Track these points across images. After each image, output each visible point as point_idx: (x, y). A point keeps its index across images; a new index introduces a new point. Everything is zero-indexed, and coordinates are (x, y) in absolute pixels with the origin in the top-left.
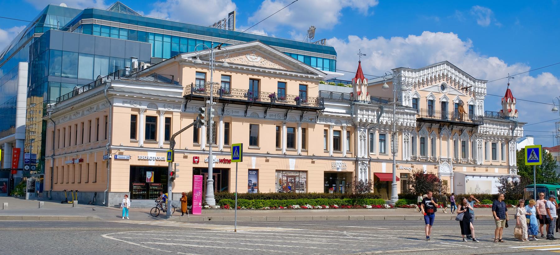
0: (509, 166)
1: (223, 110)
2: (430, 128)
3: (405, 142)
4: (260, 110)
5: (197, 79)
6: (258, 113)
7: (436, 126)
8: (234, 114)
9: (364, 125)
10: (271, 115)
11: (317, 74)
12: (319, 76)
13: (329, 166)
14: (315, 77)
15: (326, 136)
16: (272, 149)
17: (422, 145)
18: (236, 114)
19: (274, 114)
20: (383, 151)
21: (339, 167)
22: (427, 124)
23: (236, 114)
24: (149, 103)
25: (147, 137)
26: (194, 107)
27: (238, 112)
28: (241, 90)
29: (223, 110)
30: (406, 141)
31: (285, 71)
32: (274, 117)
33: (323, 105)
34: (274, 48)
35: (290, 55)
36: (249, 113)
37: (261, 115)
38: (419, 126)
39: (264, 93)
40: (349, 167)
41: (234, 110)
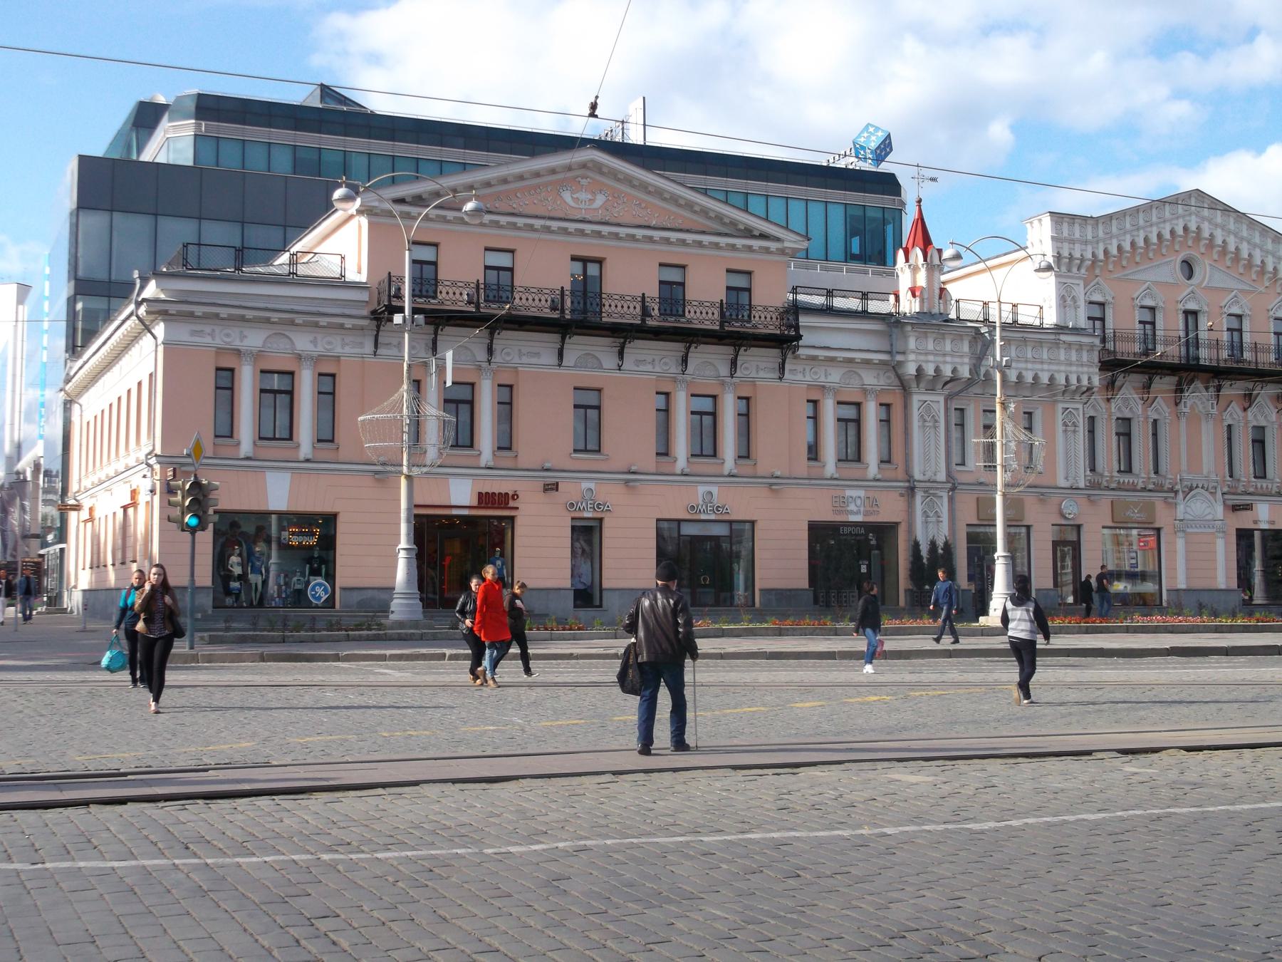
0: (909, 477)
1: (490, 351)
2: (1147, 387)
3: (1065, 431)
4: (602, 349)
5: (728, 288)
6: (597, 354)
7: (1164, 384)
8: (525, 360)
9: (936, 382)
10: (638, 362)
11: (778, 239)
12: (787, 244)
13: (674, 501)
14: (773, 246)
15: (815, 418)
16: (645, 456)
17: (744, 418)
18: (534, 360)
19: (649, 359)
20: (708, 449)
21: (856, 508)
22: (1134, 377)
23: (534, 360)
24: (271, 332)
25: (842, 460)
26: (657, 358)
27: (537, 355)
28: (540, 291)
29: (490, 351)
30: (1070, 427)
31: (726, 235)
32: (649, 368)
33: (797, 328)
34: (667, 178)
35: (705, 192)
36: (569, 358)
37: (609, 360)
38: (1111, 386)
39: (527, 289)
40: (889, 509)
41: (524, 350)
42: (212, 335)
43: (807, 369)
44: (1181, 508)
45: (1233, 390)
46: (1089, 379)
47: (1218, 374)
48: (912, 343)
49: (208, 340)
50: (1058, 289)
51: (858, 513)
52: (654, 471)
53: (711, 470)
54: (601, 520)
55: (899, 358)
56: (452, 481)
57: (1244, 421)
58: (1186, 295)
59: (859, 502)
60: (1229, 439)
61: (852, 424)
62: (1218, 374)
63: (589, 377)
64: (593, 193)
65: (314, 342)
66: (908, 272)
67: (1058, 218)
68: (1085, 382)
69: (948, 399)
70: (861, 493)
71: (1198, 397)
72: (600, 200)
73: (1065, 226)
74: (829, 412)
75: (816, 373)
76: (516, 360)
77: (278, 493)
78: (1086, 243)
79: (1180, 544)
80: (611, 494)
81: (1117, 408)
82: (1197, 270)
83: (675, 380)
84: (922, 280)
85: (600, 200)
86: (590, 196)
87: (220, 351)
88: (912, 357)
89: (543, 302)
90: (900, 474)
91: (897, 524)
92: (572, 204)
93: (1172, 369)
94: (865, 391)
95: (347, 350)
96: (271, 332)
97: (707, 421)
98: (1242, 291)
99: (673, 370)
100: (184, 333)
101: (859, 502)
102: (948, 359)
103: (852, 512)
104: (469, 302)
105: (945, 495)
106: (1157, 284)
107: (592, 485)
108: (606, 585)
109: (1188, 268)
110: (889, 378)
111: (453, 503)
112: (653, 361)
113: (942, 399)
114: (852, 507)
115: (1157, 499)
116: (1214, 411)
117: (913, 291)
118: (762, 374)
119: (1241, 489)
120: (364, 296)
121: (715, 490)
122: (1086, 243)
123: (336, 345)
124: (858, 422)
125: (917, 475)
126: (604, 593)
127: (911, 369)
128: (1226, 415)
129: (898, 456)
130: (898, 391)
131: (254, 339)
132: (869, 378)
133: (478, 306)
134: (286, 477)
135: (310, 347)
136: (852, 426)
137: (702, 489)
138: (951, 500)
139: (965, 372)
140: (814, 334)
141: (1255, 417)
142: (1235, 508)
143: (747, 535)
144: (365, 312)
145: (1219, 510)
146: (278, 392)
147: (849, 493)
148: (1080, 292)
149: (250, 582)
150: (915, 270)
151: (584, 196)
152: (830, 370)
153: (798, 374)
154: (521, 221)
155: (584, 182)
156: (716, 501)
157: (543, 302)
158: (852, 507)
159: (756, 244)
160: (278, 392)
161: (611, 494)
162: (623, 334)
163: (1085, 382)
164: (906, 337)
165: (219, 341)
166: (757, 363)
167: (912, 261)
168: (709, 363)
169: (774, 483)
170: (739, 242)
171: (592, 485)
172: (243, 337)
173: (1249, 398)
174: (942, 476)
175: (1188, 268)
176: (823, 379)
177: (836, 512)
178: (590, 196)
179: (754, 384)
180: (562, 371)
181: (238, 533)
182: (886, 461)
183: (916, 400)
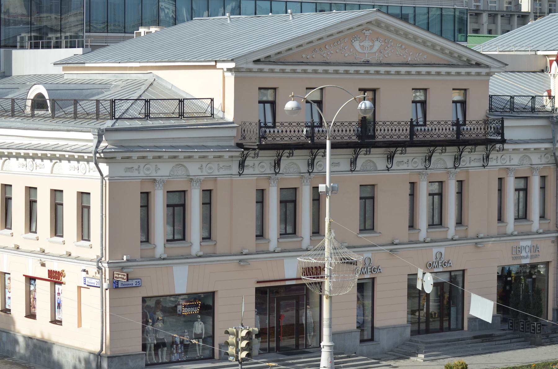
6: (373, 160)
11: (487, 67)
16: (404, 233)
24: (174, 164)
32: (405, 166)
49: (136, 174)
51: (527, 257)
52: (406, 240)
54: (373, 279)
56: (286, 261)
59: (527, 249)
61: (524, 191)
64: (373, 41)
70: (529, 243)
72: (377, 45)
74: (511, 185)
80: (379, 257)
83: (420, 174)
85: (377, 45)
86: (371, 44)
87: (143, 181)
89: (352, 132)
92: (360, 50)
95: (222, 172)
96: (174, 164)
99: (420, 167)
101: (527, 249)
104: (307, 137)
110: (547, 158)
111: (287, 277)
112: (410, 161)
114: (524, 254)
118: (473, 164)
120: (234, 133)
123: (215, 169)
124: (525, 190)
126: (375, 330)
131: (164, 170)
133: (312, 140)
134: (186, 267)
135: (198, 172)
143: (460, 279)
144: (233, 143)
146: (177, 207)
147: (523, 244)
151: (367, 43)
155: (367, 33)
156: (445, 259)
157: (352, 132)
158: (524, 254)
159: (474, 70)
160: (177, 207)
161: (379, 257)
162: (393, 146)
165: (143, 173)
168: (443, 159)
170: (463, 70)
171: (369, 255)
172: (157, 169)
176: (508, 163)
178: (371, 44)
180: (354, 174)
181: (156, 308)
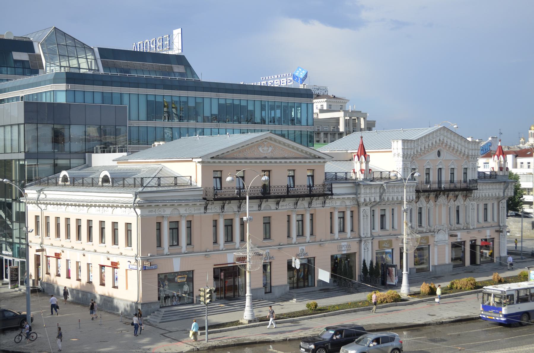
0: (360, 237)
2: (428, 197)
11: (324, 158)
16: (284, 239)
19: (285, 204)
32: (285, 208)
36: (263, 206)
38: (418, 198)
40: (354, 249)
42: (155, 211)
43: (157, 209)
44: (436, 238)
45: (451, 194)
46: (375, 198)
47: (446, 191)
48: (363, 191)
49: (154, 213)
50: (403, 165)
52: (286, 243)
53: (303, 241)
55: (359, 196)
56: (228, 254)
57: (453, 204)
58: (439, 163)
60: (393, 214)
62: (446, 191)
63: (267, 213)
65: (186, 210)
66: (358, 164)
67: (404, 141)
68: (411, 198)
69: (371, 208)
70: (346, 243)
71: (442, 199)
72: (270, 149)
73: (406, 144)
74: (336, 215)
75: (160, 211)
76: (193, 212)
77: (177, 265)
78: (411, 149)
79: (436, 249)
80: (273, 252)
81: (419, 205)
82: (442, 153)
83: (292, 211)
84: (364, 167)
85: (270, 149)
87: (157, 217)
88: (363, 196)
90: (357, 236)
91: (355, 253)
93: (434, 191)
94: (346, 207)
95: (196, 212)
97: (229, 226)
98: (455, 160)
100: (146, 212)
102: (368, 195)
103: (343, 251)
105: (370, 241)
106: (431, 160)
107: (268, 251)
108: (273, 284)
109: (439, 154)
112: (287, 205)
113: (369, 208)
114: (343, 249)
115: (429, 235)
116: (446, 203)
117: (361, 170)
118: (318, 206)
119: (453, 228)
120: (201, 193)
121: (304, 248)
122: (411, 149)
125: (362, 236)
127: (362, 200)
128: (449, 204)
129: (356, 229)
130: (356, 206)
131: (168, 211)
132: (348, 203)
134: (179, 259)
136: (342, 219)
137: (300, 248)
138: (372, 243)
139: (378, 199)
140: (337, 189)
141: (457, 203)
142: (451, 236)
144: (201, 198)
145: (447, 236)
146: (175, 229)
147: (343, 244)
148: (409, 165)
149: (169, 296)
150: (361, 163)
151: (265, 148)
152: (166, 209)
153: (329, 203)
154: (248, 161)
155: (265, 143)
156: (305, 252)
158: (343, 249)
159: (317, 160)
160: (175, 229)
162: (279, 198)
163: (411, 198)
164: (360, 189)
165: (157, 213)
166: (317, 203)
167: (360, 160)
168: (303, 203)
169: (321, 243)
170: (312, 161)
171: (268, 251)
173: (456, 197)
174: (369, 235)
175: (439, 154)
177: (339, 251)
179: (315, 209)
180: (260, 212)
181: (165, 279)
182: (352, 231)
183: (362, 209)
